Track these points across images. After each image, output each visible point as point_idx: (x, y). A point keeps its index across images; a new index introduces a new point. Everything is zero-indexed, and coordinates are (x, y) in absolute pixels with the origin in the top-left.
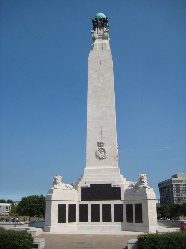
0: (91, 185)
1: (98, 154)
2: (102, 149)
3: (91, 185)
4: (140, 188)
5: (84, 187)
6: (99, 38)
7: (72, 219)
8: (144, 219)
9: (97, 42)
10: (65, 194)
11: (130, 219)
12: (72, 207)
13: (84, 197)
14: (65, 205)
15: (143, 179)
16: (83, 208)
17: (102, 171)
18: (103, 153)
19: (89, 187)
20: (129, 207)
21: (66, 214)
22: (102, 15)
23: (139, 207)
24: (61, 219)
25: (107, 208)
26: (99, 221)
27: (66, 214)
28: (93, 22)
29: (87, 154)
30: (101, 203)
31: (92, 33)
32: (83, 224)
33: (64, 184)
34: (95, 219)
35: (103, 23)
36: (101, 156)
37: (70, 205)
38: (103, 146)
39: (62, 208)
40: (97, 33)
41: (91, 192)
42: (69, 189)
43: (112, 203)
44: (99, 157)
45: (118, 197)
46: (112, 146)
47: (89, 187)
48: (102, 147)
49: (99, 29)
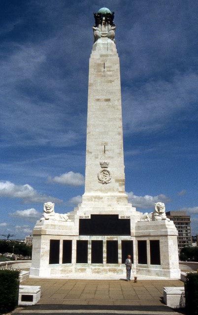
0: (92, 216)
1: (100, 177)
2: (105, 171)
3: (92, 216)
4: (157, 220)
5: (84, 218)
6: (102, 36)
7: (67, 259)
8: (162, 257)
9: (99, 41)
10: (62, 225)
11: (142, 260)
12: (68, 244)
13: (82, 231)
14: (58, 241)
15: (161, 209)
16: (82, 245)
17: (105, 196)
18: (108, 176)
19: (90, 218)
20: (142, 245)
21: (59, 252)
22: (105, 10)
23: (155, 245)
24: (54, 260)
25: (112, 245)
26: (86, 262)
27: (59, 252)
28: (96, 17)
29: (121, 180)
30: (104, 239)
31: (94, 30)
32: (97, 266)
33: (57, 214)
34: (97, 259)
35: (110, 19)
36: (104, 180)
37: (151, 242)
38: (107, 168)
39: (54, 244)
40: (101, 30)
41: (88, 225)
42: (63, 220)
43: (120, 239)
44: (102, 181)
45: (128, 232)
46: (117, 169)
47: (90, 218)
48: (106, 169)
49: (103, 26)
